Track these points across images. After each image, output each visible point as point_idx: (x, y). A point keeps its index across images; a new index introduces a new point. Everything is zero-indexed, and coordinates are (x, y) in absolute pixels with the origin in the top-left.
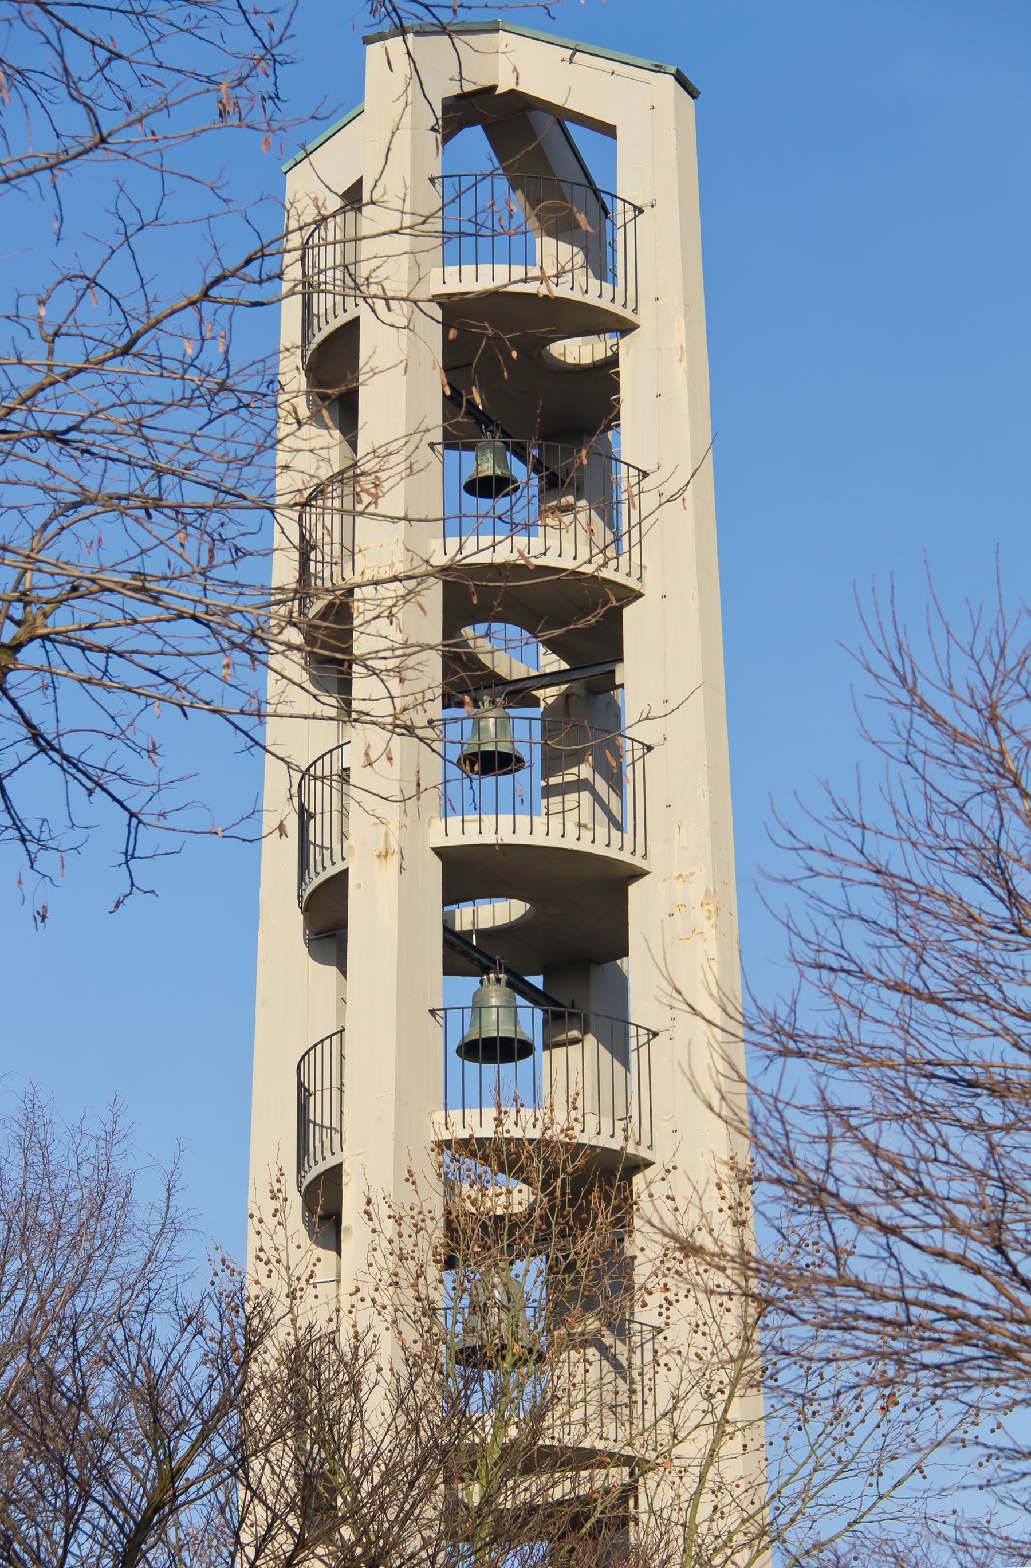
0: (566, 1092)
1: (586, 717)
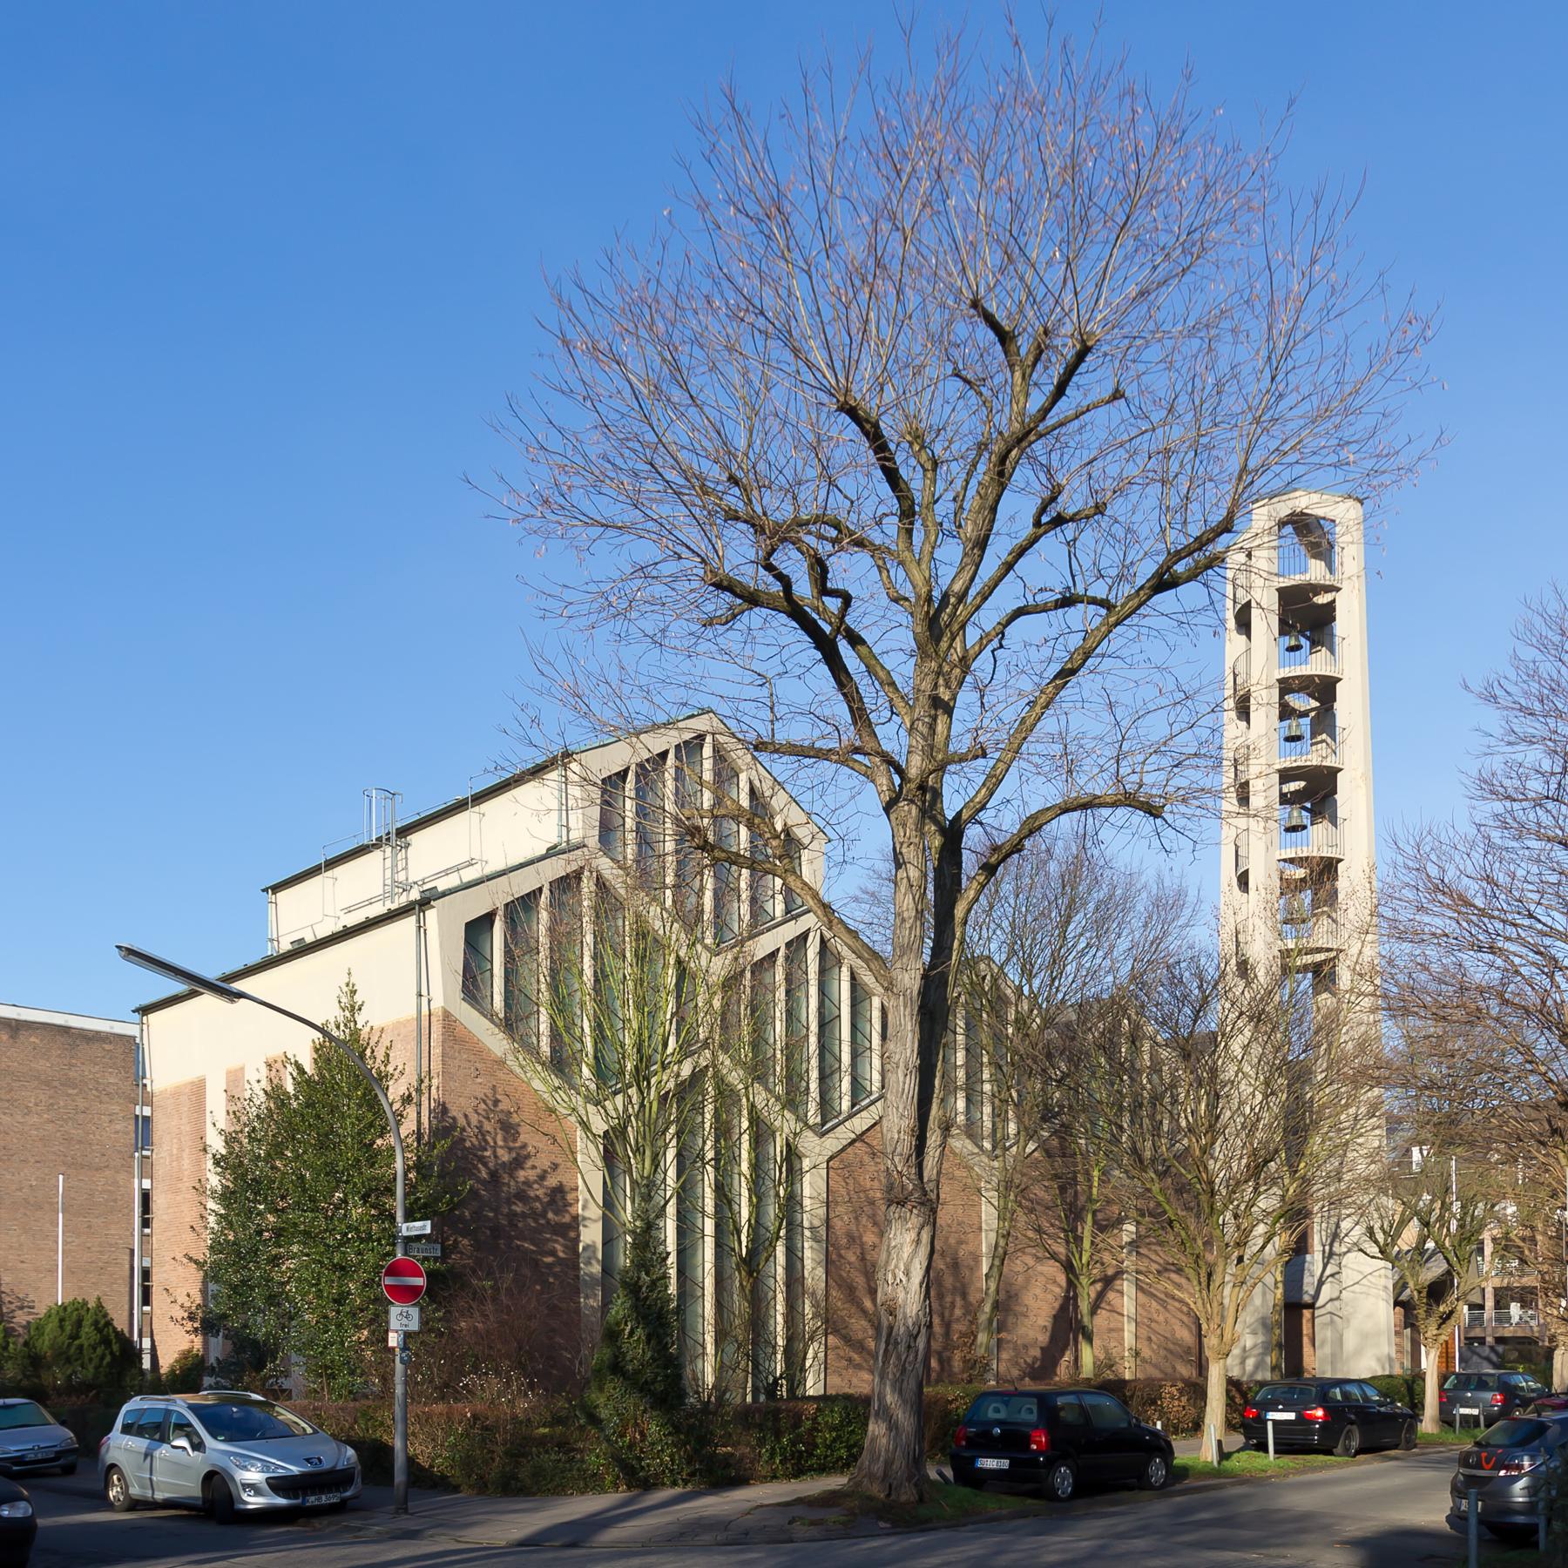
0: (1317, 841)
1: (1324, 721)
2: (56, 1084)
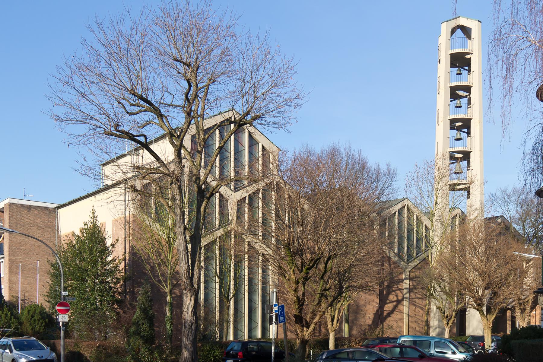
2: (43, 227)
